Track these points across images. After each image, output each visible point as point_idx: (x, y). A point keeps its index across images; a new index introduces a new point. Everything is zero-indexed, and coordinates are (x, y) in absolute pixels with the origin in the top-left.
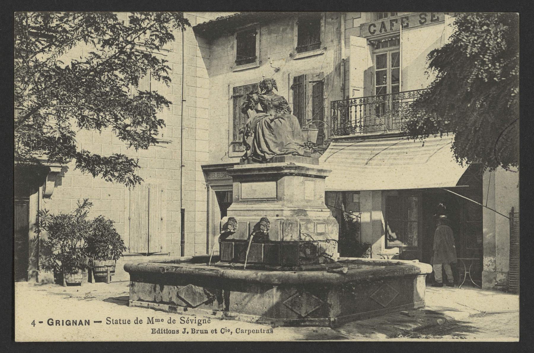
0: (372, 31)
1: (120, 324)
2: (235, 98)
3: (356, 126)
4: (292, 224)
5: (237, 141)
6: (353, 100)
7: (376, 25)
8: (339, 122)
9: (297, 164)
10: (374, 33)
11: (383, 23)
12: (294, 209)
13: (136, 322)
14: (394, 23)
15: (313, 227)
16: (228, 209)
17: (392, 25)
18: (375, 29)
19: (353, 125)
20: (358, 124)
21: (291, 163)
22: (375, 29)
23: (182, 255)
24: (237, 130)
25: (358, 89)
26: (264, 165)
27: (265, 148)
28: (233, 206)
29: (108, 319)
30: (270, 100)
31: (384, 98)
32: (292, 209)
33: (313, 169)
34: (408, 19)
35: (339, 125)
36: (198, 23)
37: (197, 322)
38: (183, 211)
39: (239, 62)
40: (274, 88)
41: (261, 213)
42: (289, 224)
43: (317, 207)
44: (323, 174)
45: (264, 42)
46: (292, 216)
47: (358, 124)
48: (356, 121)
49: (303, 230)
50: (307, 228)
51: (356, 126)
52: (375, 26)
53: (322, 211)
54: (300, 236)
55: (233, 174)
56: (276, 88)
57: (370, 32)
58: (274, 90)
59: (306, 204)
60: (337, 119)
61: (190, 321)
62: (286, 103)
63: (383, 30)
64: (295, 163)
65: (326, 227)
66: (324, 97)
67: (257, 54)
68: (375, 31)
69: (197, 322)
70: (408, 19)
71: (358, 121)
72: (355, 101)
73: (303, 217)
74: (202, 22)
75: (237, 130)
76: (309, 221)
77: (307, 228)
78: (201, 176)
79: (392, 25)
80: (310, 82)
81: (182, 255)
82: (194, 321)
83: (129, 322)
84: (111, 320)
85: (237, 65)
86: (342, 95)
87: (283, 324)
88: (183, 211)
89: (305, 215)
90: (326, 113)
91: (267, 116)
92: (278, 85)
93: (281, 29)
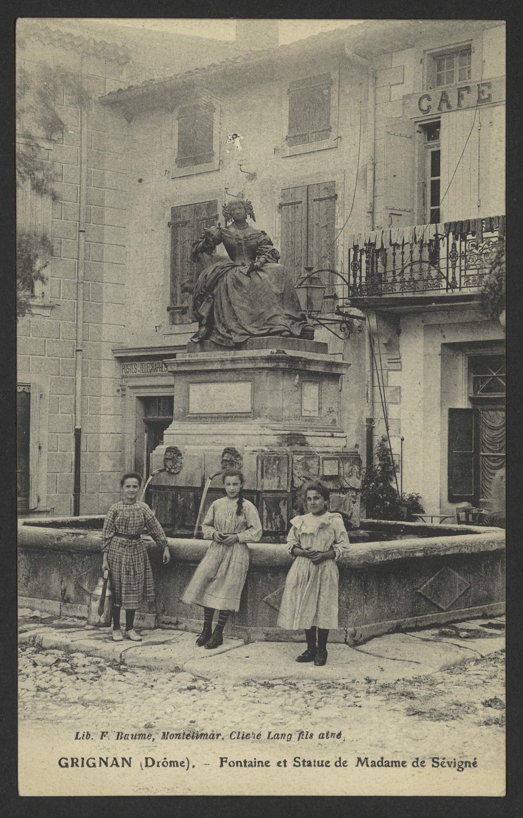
0: (425, 108)
1: (315, 766)
2: (175, 226)
3: (395, 281)
4: (279, 459)
5: (178, 305)
7: (432, 97)
8: (364, 274)
9: (290, 353)
10: (428, 111)
11: (444, 94)
12: (283, 432)
14: (465, 93)
15: (315, 465)
16: (165, 432)
17: (460, 97)
18: (430, 103)
19: (390, 280)
20: (398, 279)
21: (278, 352)
22: (430, 103)
23: (77, 513)
24: (178, 286)
25: (399, 213)
26: (229, 355)
27: (233, 325)
28: (174, 427)
29: (297, 759)
30: (242, 236)
32: (278, 432)
34: (489, 87)
35: (363, 280)
38: (78, 433)
40: (248, 216)
41: (224, 439)
42: (275, 459)
43: (324, 429)
44: (334, 370)
46: (280, 444)
47: (398, 279)
48: (394, 273)
49: (299, 472)
50: (307, 468)
51: (395, 281)
52: (429, 99)
53: (332, 436)
54: (293, 481)
56: (253, 217)
57: (421, 110)
58: (249, 220)
59: (306, 424)
60: (360, 268)
62: (270, 243)
63: (444, 105)
64: (286, 351)
65: (341, 464)
66: (337, 227)
67: (216, 149)
68: (429, 107)
70: (489, 87)
71: (398, 272)
73: (297, 448)
75: (178, 286)
76: (310, 455)
77: (307, 468)
78: (109, 369)
79: (460, 97)
80: (315, 200)
81: (77, 513)
84: (300, 761)
85: (179, 167)
86: (370, 222)
87: (263, 637)
88: (78, 433)
89: (303, 444)
90: (340, 255)
91: (234, 266)
92: (255, 212)
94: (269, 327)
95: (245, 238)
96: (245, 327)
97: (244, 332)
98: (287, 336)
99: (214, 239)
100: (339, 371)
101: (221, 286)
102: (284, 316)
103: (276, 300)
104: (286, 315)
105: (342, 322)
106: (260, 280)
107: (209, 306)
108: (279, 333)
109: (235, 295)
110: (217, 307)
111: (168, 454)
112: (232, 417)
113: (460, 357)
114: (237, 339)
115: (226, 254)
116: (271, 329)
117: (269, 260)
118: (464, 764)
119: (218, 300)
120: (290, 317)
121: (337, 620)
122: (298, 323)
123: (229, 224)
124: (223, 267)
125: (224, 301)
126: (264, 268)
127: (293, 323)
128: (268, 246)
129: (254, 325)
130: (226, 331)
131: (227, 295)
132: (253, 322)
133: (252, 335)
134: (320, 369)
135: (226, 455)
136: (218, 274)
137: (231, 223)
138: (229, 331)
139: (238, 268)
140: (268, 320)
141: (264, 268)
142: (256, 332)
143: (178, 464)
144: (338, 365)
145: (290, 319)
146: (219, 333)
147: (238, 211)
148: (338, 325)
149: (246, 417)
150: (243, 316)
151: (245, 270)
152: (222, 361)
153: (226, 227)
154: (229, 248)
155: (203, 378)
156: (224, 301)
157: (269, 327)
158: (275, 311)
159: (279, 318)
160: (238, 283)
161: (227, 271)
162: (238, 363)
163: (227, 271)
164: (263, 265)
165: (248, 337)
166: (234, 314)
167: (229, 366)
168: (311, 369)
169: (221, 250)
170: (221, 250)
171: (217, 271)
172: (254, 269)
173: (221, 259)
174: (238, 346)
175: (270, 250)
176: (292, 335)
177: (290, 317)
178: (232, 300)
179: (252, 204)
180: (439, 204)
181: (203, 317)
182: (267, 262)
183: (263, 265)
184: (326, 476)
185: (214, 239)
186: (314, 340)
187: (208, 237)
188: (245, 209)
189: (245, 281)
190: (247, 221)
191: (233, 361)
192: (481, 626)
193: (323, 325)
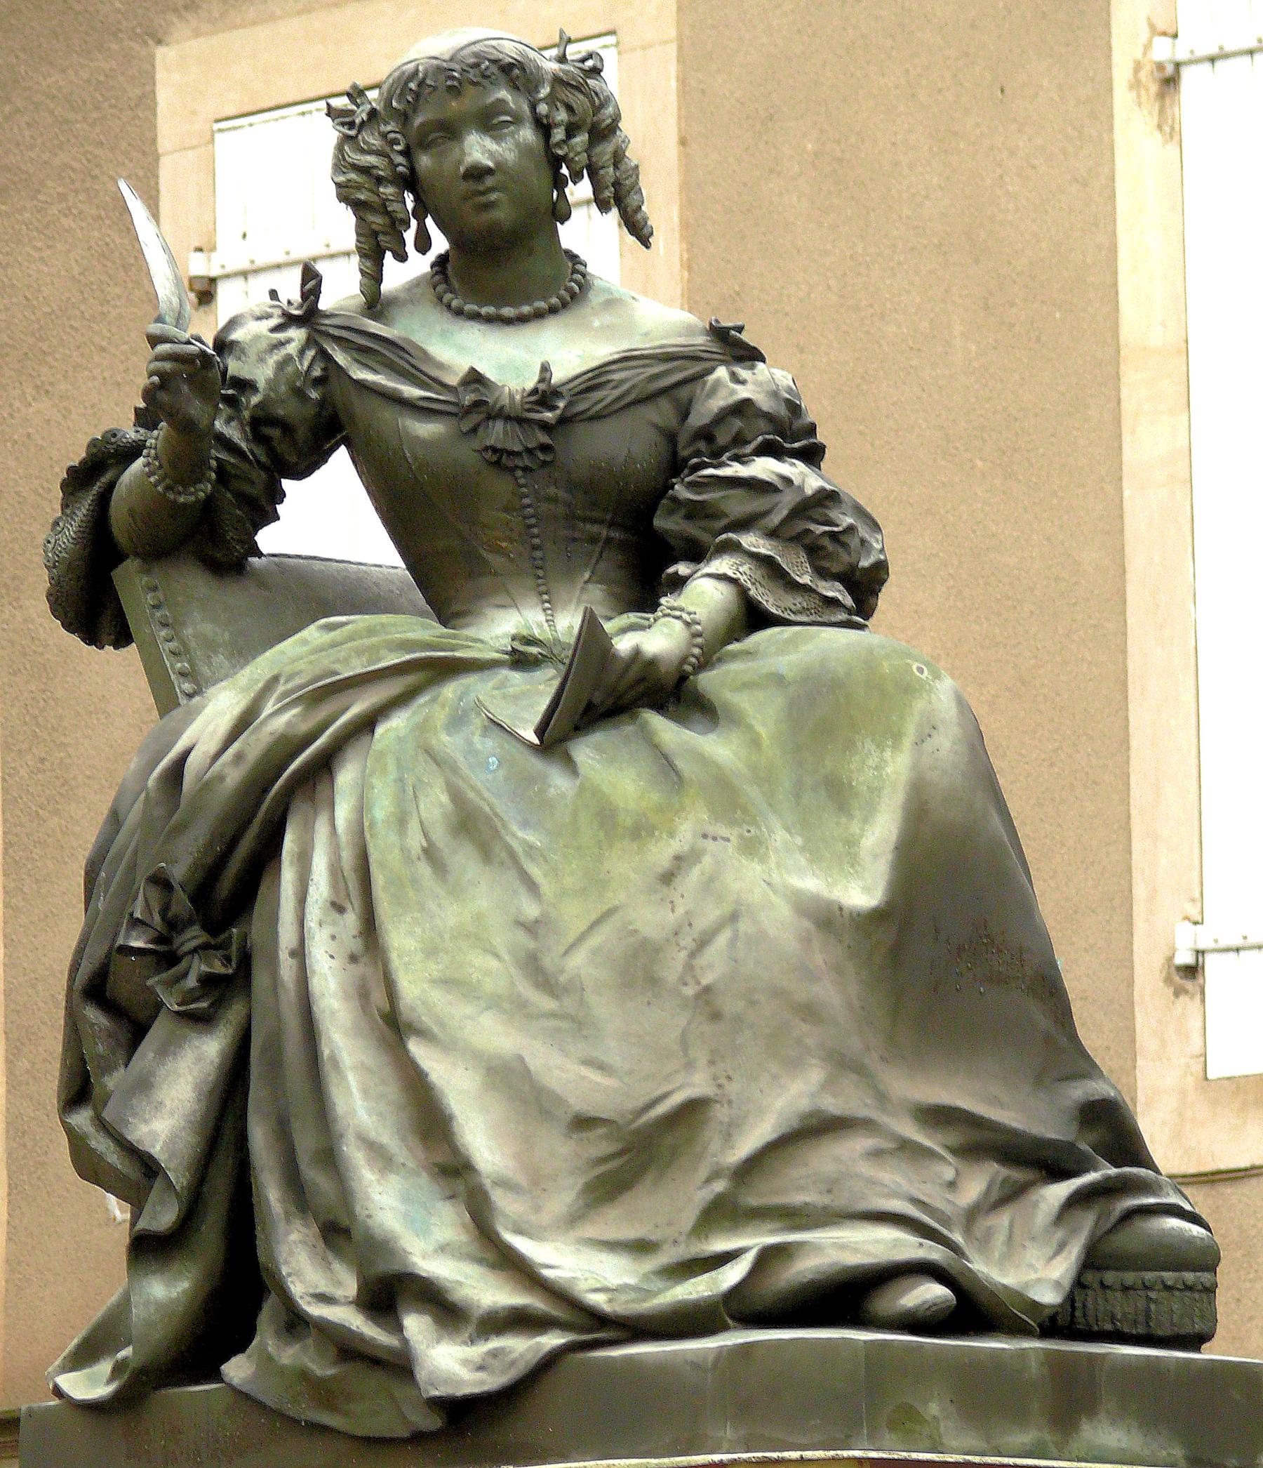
27: (429, 1243)
58: (588, 233)
94: (754, 1240)
99: (260, 424)
104: (938, 1116)
107: (206, 1052)
110: (275, 1064)
113: (511, 1163)
116: (769, 1257)
117: (770, 601)
120: (982, 1141)
122: (1059, 1191)
123: (399, 275)
130: (349, 1286)
136: (290, 746)
137: (419, 265)
146: (295, 1323)
147: (478, 149)
153: (375, 303)
154: (403, 500)
159: (853, 1147)
163: (367, 724)
164: (709, 649)
165: (552, 1340)
169: (328, 517)
171: (279, 721)
177: (982, 1141)
179: (613, 80)
181: (149, 1167)
182: (753, 618)
185: (260, 424)
187: (196, 408)
188: (544, 127)
190: (570, 235)
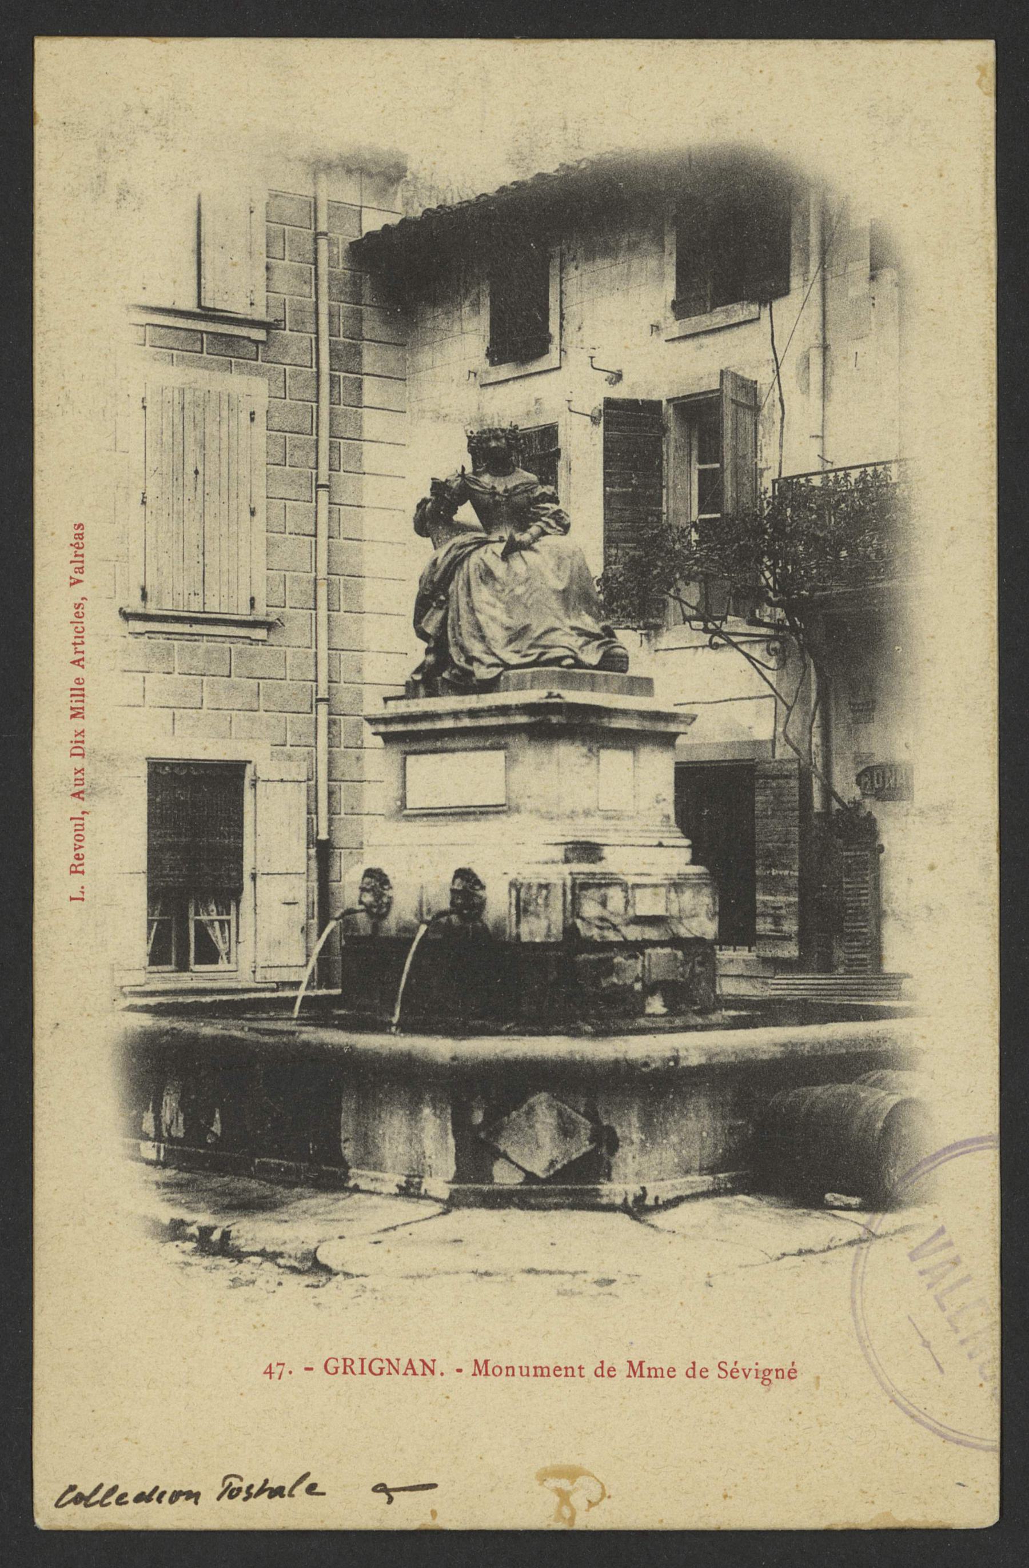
6: (841, 474)
13: (691, 1373)
21: (550, 695)
26: (472, 701)
27: (477, 649)
29: (723, 1365)
30: (500, 489)
31: (735, 447)
33: (625, 713)
36: (364, 232)
37: (761, 1375)
39: (497, 354)
45: (571, 287)
55: (382, 728)
61: (741, 1373)
64: (564, 693)
69: (761, 1375)
72: (847, 475)
74: (377, 227)
82: (753, 1373)
83: (671, 1373)
93: (624, 243)
94: (539, 651)
95: (506, 491)
96: (497, 652)
97: (496, 661)
98: (569, 667)
100: (673, 728)
101: (460, 578)
102: (568, 630)
103: (555, 604)
104: (573, 628)
105: (768, 639)
106: (524, 567)
107: (439, 615)
108: (557, 661)
109: (483, 595)
111: (367, 880)
112: (474, 813)
114: (482, 673)
115: (474, 520)
116: (542, 654)
117: (549, 530)
118: (774, 1373)
119: (453, 606)
120: (581, 632)
121: (133, 899)
122: (597, 643)
124: (463, 546)
125: (463, 605)
126: (536, 545)
127: (587, 643)
128: (547, 505)
129: (511, 648)
131: (469, 594)
132: (510, 641)
133: (507, 667)
134: (633, 724)
135: (458, 881)
138: (471, 660)
139: (491, 546)
140: (539, 637)
141: (536, 545)
142: (515, 659)
143: (385, 900)
144: (670, 717)
145: (580, 635)
148: (764, 645)
149: (498, 813)
150: (496, 634)
151: (499, 548)
152: (456, 715)
155: (428, 745)
156: (463, 605)
157: (539, 651)
158: (551, 622)
160: (488, 575)
161: (470, 552)
162: (482, 717)
163: (470, 552)
165: (501, 669)
166: (479, 628)
167: (466, 722)
168: (613, 725)
170: (466, 514)
172: (512, 548)
173: (463, 528)
174: (490, 686)
175: (551, 512)
176: (579, 664)
177: (581, 632)
178: (477, 605)
180: (555, 483)
182: (544, 533)
183: (536, 539)
184: (641, 917)
186: (628, 674)
188: (507, 439)
189: (499, 569)
191: (473, 713)
192: (319, 936)
193: (735, 645)
